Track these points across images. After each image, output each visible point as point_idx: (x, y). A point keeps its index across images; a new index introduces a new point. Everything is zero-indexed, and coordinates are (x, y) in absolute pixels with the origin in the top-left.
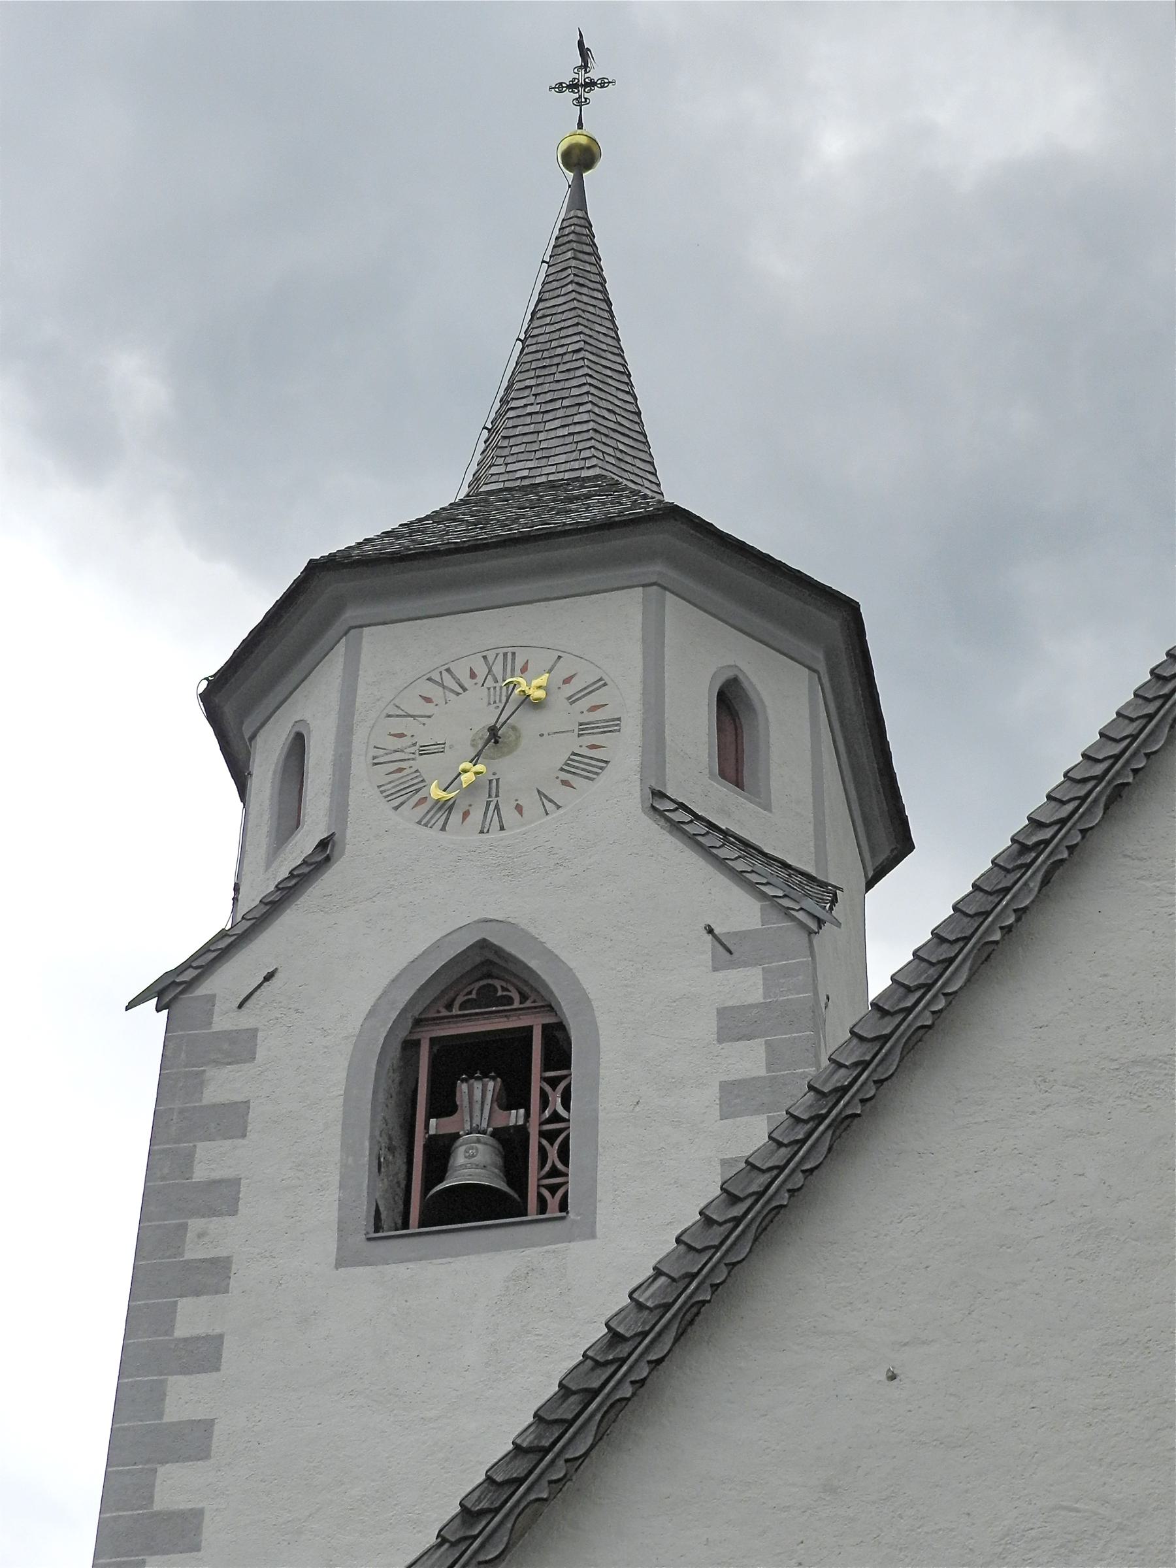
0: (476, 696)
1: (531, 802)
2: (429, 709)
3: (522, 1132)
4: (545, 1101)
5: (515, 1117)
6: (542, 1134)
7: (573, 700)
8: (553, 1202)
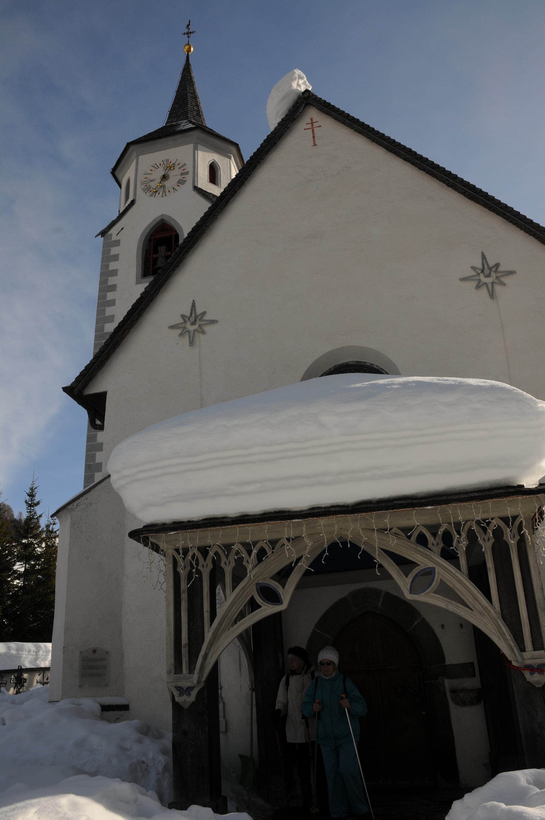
1: (171, 190)
2: (152, 172)
7: (179, 168)
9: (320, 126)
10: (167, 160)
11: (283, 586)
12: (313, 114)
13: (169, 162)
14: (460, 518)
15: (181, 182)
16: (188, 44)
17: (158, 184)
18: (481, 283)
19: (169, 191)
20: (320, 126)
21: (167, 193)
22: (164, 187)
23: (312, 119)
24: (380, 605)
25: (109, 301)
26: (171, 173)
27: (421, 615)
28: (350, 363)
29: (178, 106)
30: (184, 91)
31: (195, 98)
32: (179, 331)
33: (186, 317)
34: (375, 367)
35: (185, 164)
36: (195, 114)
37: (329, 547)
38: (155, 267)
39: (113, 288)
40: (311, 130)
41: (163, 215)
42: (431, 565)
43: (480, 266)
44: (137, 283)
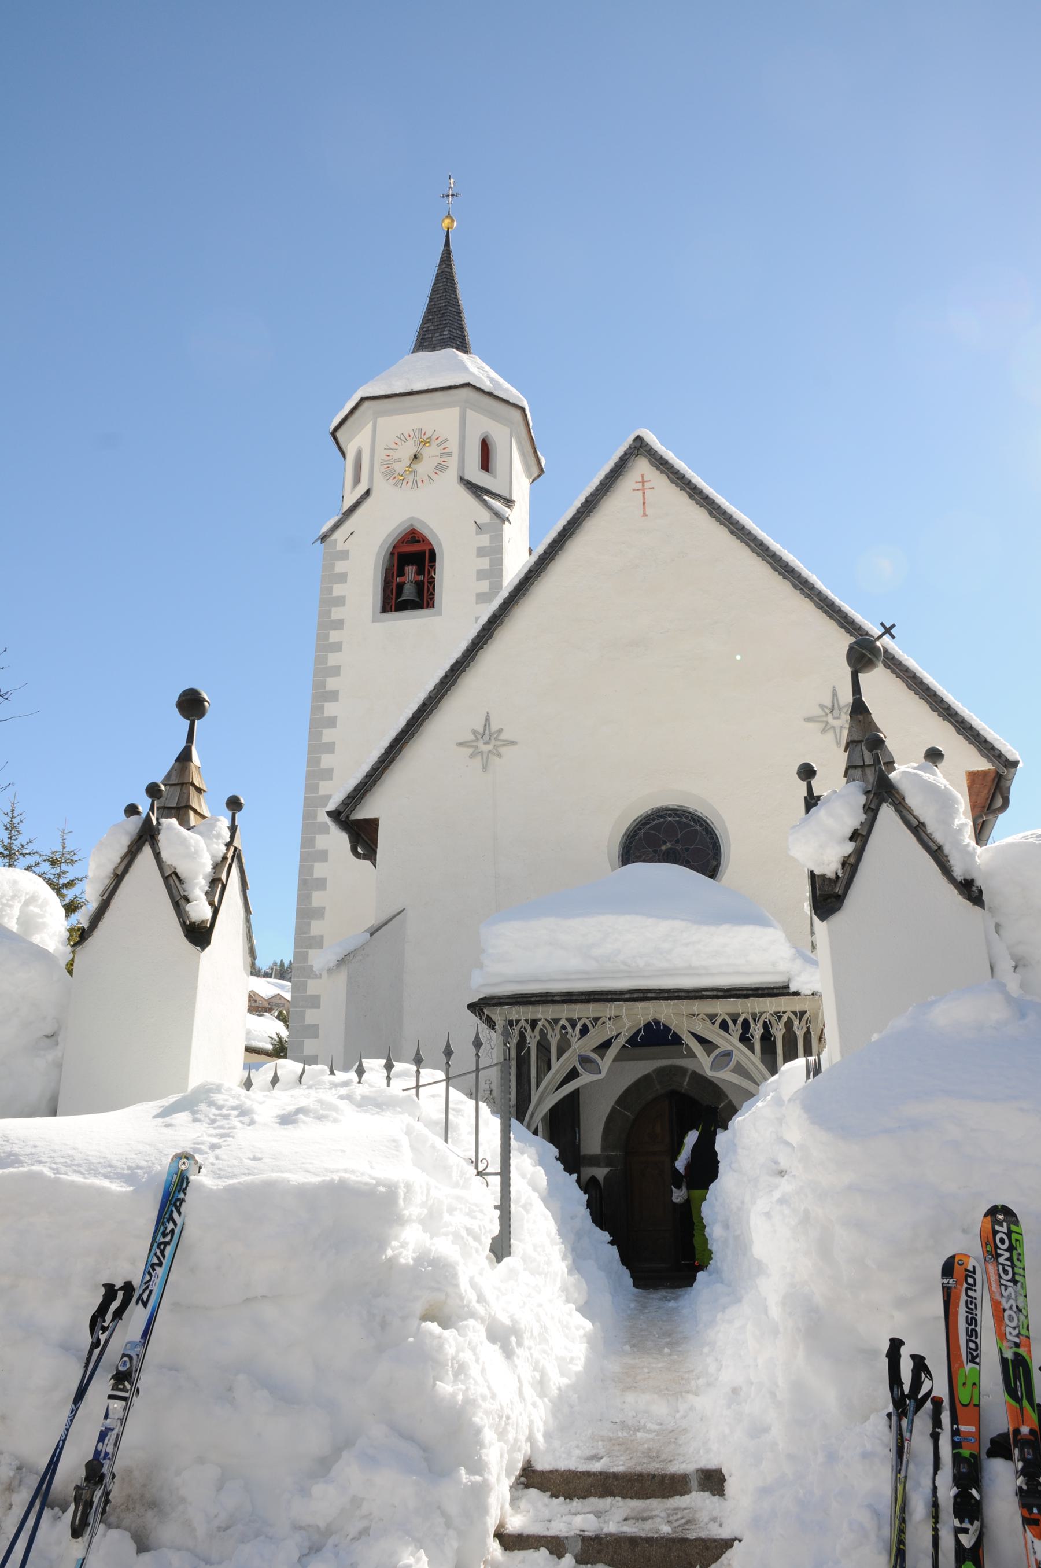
0: (411, 442)
1: (426, 479)
2: (396, 447)
3: (423, 582)
4: (429, 572)
5: (421, 578)
6: (428, 582)
7: (438, 445)
8: (431, 603)
9: (653, 488)
10: (420, 430)
11: (602, 1059)
12: (642, 467)
13: (423, 433)
14: (757, 1011)
15: (441, 468)
16: (449, 216)
17: (407, 469)
18: (828, 727)
19: (422, 481)
20: (653, 488)
21: (420, 483)
22: (415, 472)
23: (642, 476)
24: (686, 1083)
25: (331, 643)
26: (427, 452)
27: (727, 1097)
28: (671, 807)
29: (432, 328)
30: (442, 301)
31: (459, 322)
32: (471, 750)
33: (479, 733)
34: (700, 814)
35: (447, 440)
36: (458, 343)
37: (644, 1026)
38: (401, 599)
39: (339, 624)
40: (640, 493)
41: (412, 518)
42: (730, 1048)
43: (830, 705)
44: (373, 621)
